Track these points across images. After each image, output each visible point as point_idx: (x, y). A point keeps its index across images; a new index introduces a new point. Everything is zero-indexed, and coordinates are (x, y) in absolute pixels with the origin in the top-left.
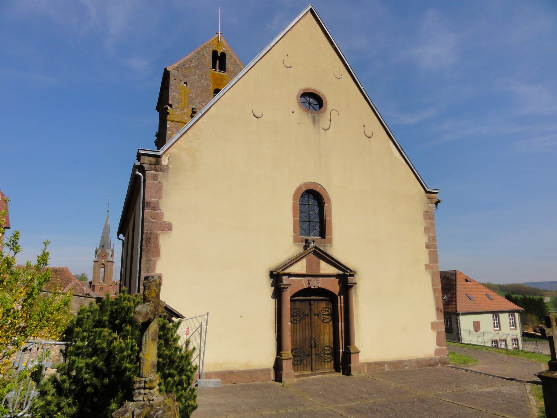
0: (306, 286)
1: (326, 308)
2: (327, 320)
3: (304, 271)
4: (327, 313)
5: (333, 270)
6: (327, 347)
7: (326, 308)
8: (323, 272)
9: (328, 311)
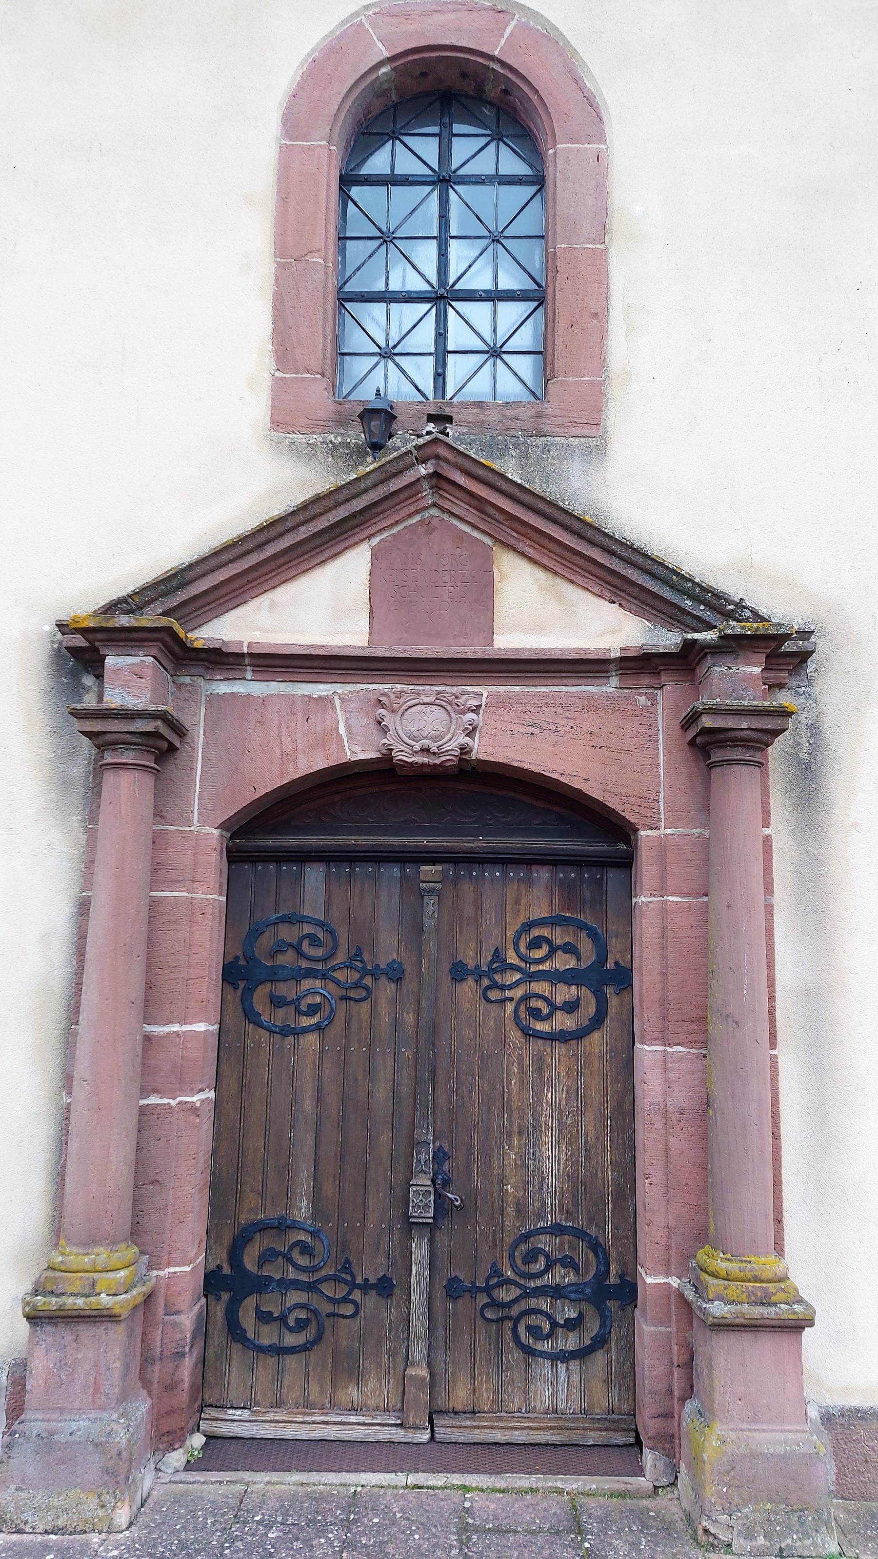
0: (358, 749)
1: (553, 921)
2: (563, 1021)
3: (352, 635)
4: (564, 962)
5: (608, 627)
6: (557, 1230)
7: (553, 921)
8: (509, 640)
9: (570, 949)
